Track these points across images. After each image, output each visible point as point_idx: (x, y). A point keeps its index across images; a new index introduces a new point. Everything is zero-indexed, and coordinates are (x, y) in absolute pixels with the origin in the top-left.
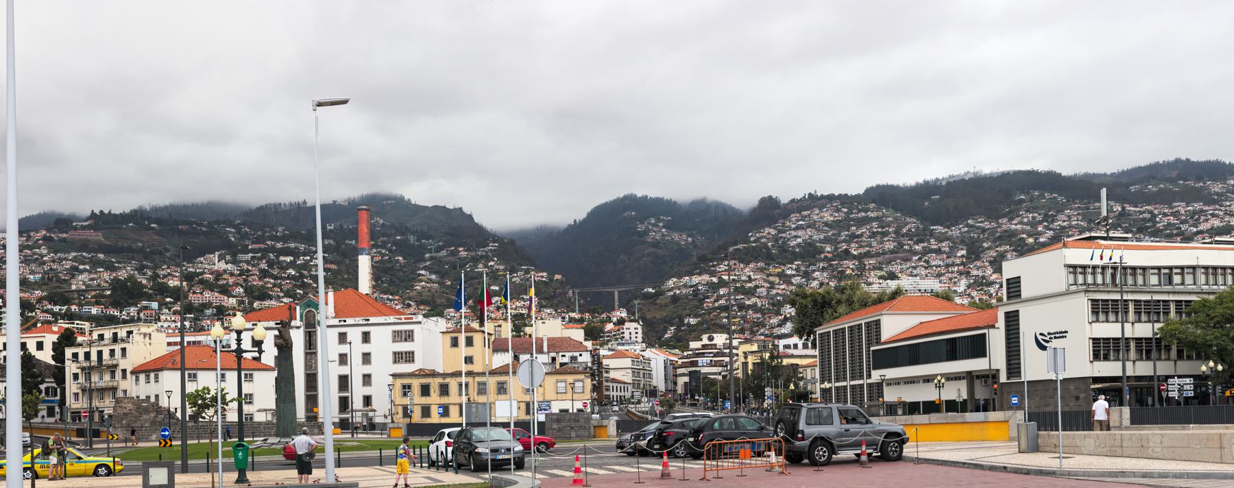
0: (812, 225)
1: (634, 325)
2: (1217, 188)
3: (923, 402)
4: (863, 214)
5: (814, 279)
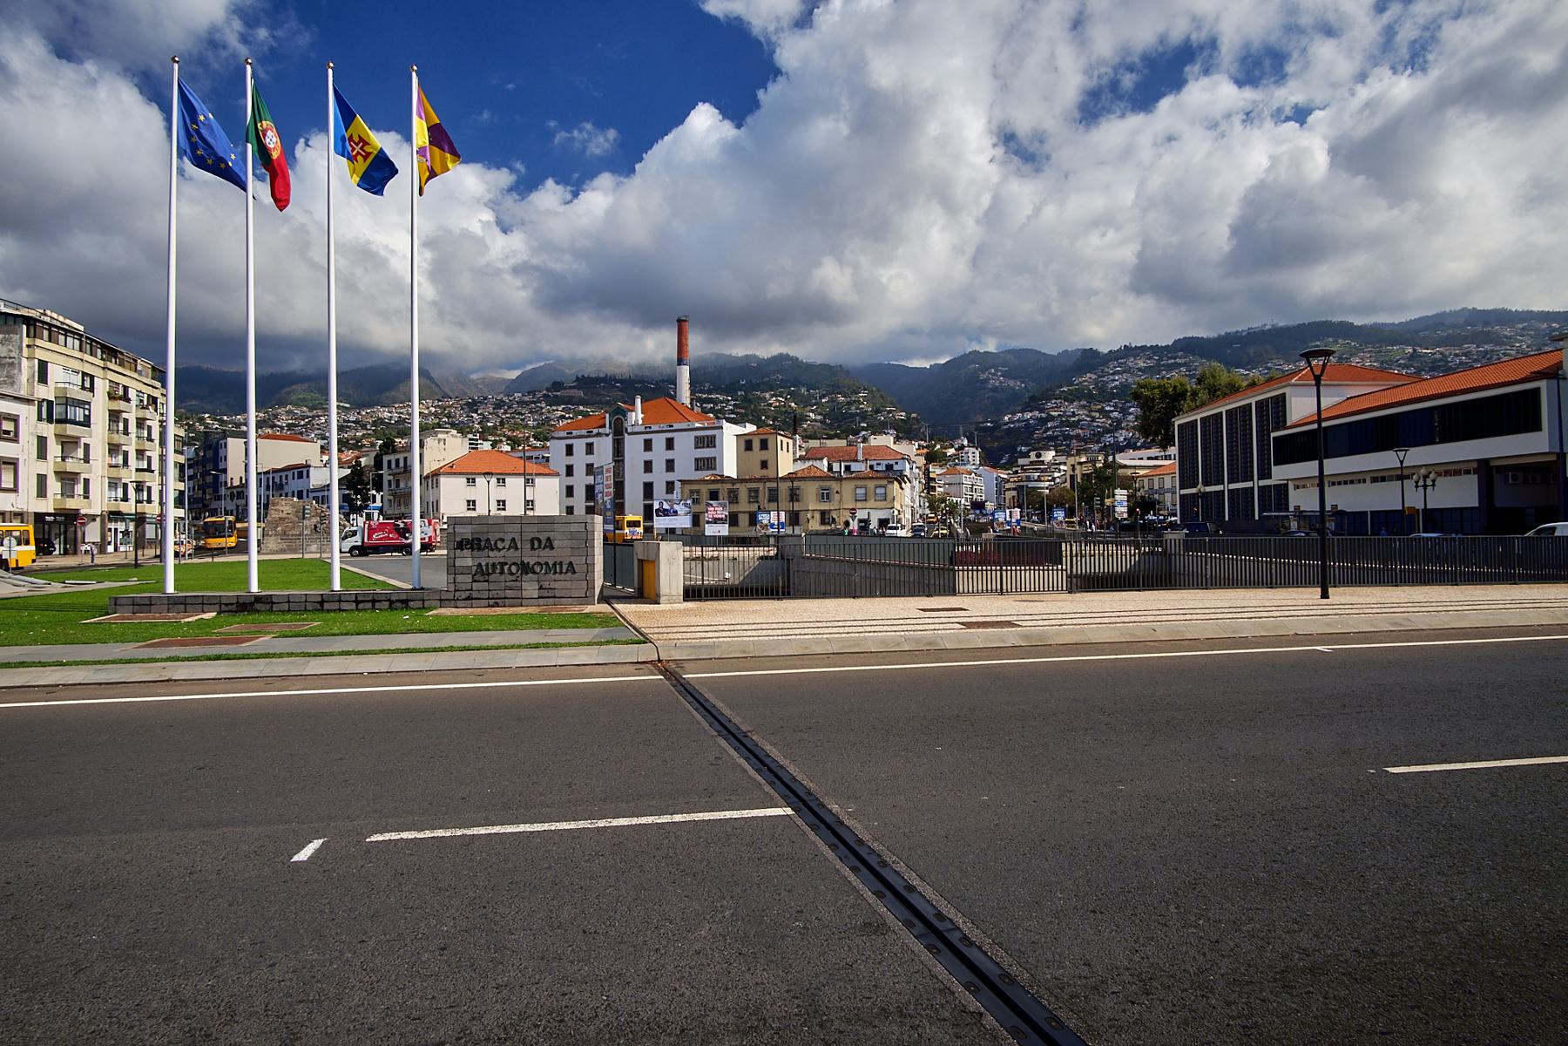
0: (1128, 371)
1: (973, 450)
2: (1507, 332)
3: (1371, 512)
4: (1173, 361)
5: (1130, 414)
